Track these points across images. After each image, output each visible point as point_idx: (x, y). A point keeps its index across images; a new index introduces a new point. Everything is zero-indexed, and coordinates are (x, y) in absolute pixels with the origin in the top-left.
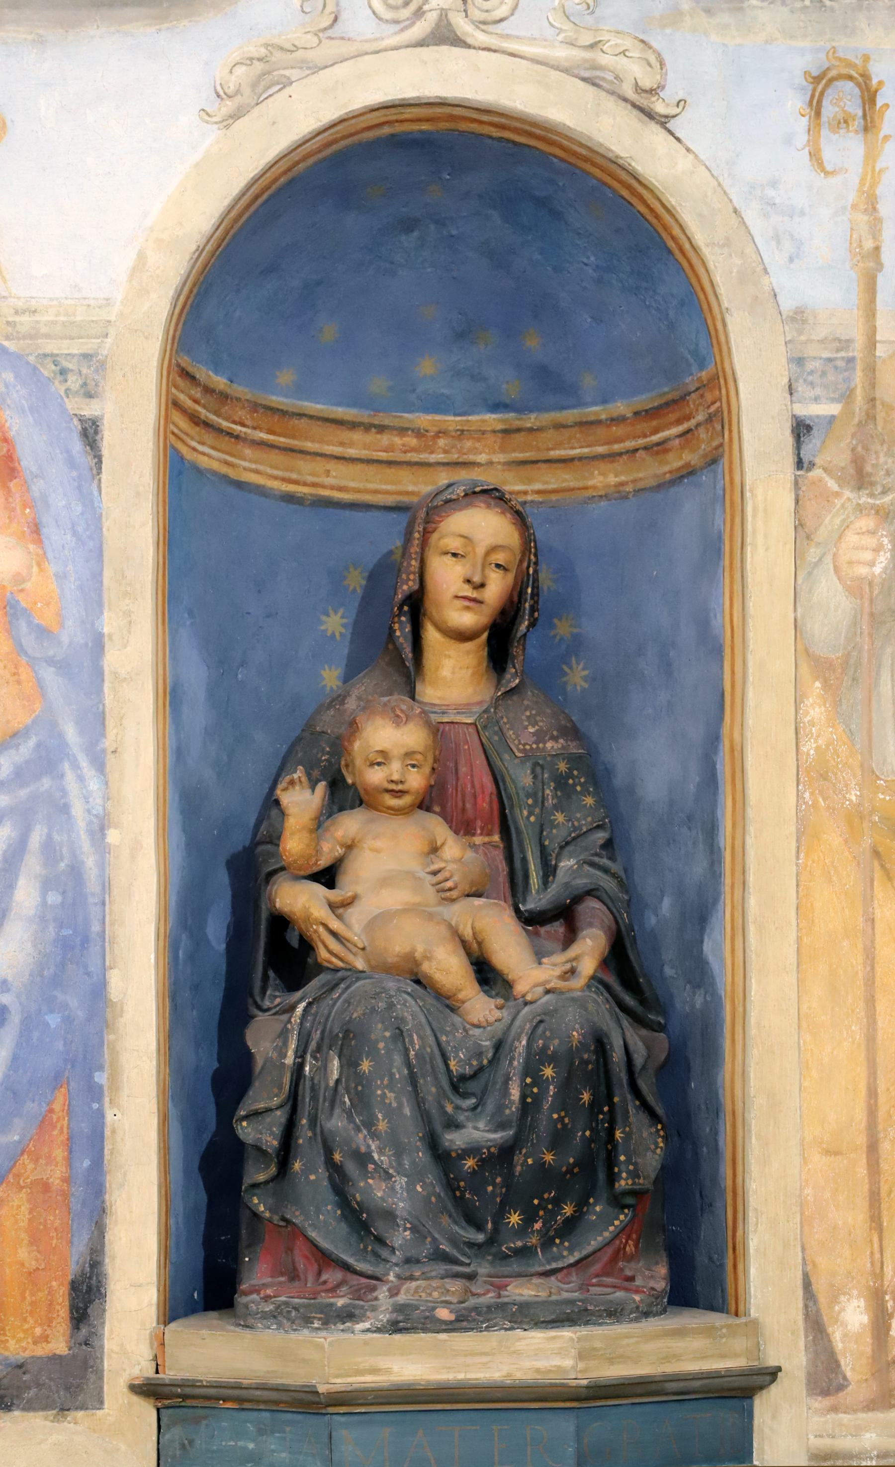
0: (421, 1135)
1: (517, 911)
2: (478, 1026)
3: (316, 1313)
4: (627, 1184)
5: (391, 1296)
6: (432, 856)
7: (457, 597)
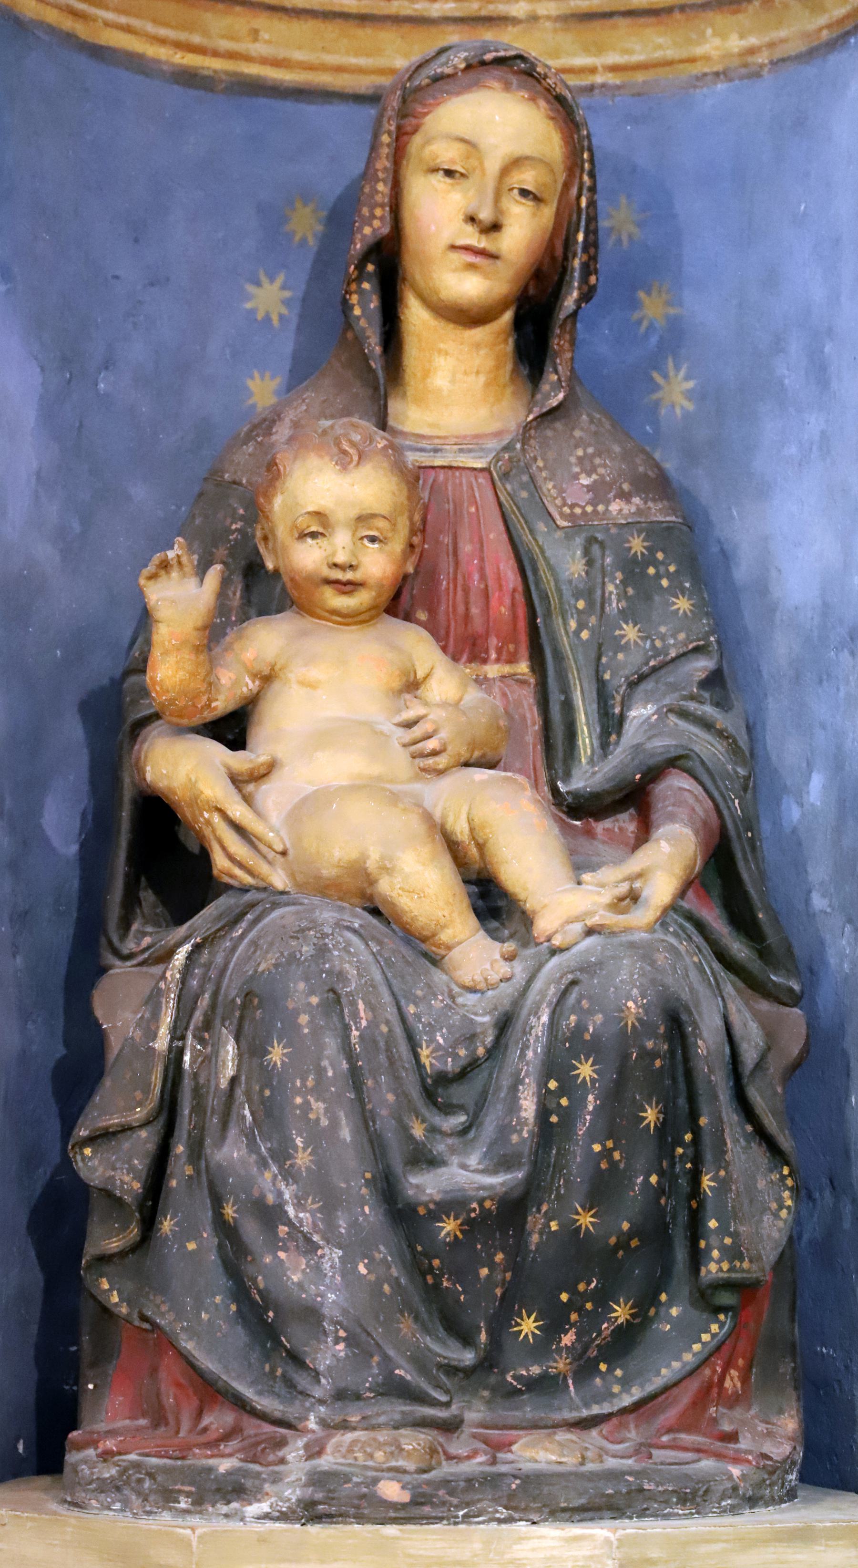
0: (368, 1175)
1: (555, 791)
2: (472, 990)
3: (182, 1484)
4: (720, 1270)
5: (309, 1457)
6: (407, 696)
7: (453, 247)
